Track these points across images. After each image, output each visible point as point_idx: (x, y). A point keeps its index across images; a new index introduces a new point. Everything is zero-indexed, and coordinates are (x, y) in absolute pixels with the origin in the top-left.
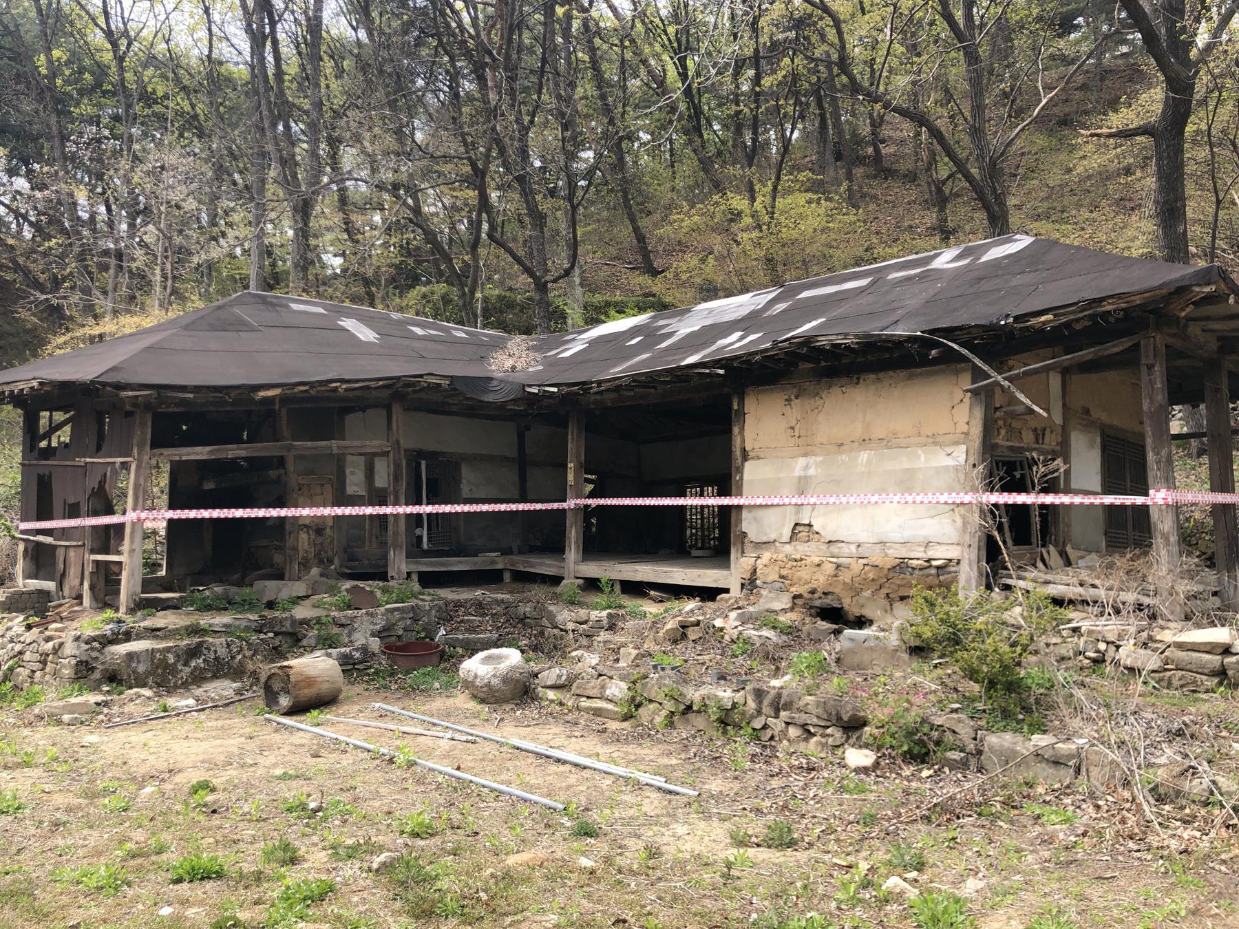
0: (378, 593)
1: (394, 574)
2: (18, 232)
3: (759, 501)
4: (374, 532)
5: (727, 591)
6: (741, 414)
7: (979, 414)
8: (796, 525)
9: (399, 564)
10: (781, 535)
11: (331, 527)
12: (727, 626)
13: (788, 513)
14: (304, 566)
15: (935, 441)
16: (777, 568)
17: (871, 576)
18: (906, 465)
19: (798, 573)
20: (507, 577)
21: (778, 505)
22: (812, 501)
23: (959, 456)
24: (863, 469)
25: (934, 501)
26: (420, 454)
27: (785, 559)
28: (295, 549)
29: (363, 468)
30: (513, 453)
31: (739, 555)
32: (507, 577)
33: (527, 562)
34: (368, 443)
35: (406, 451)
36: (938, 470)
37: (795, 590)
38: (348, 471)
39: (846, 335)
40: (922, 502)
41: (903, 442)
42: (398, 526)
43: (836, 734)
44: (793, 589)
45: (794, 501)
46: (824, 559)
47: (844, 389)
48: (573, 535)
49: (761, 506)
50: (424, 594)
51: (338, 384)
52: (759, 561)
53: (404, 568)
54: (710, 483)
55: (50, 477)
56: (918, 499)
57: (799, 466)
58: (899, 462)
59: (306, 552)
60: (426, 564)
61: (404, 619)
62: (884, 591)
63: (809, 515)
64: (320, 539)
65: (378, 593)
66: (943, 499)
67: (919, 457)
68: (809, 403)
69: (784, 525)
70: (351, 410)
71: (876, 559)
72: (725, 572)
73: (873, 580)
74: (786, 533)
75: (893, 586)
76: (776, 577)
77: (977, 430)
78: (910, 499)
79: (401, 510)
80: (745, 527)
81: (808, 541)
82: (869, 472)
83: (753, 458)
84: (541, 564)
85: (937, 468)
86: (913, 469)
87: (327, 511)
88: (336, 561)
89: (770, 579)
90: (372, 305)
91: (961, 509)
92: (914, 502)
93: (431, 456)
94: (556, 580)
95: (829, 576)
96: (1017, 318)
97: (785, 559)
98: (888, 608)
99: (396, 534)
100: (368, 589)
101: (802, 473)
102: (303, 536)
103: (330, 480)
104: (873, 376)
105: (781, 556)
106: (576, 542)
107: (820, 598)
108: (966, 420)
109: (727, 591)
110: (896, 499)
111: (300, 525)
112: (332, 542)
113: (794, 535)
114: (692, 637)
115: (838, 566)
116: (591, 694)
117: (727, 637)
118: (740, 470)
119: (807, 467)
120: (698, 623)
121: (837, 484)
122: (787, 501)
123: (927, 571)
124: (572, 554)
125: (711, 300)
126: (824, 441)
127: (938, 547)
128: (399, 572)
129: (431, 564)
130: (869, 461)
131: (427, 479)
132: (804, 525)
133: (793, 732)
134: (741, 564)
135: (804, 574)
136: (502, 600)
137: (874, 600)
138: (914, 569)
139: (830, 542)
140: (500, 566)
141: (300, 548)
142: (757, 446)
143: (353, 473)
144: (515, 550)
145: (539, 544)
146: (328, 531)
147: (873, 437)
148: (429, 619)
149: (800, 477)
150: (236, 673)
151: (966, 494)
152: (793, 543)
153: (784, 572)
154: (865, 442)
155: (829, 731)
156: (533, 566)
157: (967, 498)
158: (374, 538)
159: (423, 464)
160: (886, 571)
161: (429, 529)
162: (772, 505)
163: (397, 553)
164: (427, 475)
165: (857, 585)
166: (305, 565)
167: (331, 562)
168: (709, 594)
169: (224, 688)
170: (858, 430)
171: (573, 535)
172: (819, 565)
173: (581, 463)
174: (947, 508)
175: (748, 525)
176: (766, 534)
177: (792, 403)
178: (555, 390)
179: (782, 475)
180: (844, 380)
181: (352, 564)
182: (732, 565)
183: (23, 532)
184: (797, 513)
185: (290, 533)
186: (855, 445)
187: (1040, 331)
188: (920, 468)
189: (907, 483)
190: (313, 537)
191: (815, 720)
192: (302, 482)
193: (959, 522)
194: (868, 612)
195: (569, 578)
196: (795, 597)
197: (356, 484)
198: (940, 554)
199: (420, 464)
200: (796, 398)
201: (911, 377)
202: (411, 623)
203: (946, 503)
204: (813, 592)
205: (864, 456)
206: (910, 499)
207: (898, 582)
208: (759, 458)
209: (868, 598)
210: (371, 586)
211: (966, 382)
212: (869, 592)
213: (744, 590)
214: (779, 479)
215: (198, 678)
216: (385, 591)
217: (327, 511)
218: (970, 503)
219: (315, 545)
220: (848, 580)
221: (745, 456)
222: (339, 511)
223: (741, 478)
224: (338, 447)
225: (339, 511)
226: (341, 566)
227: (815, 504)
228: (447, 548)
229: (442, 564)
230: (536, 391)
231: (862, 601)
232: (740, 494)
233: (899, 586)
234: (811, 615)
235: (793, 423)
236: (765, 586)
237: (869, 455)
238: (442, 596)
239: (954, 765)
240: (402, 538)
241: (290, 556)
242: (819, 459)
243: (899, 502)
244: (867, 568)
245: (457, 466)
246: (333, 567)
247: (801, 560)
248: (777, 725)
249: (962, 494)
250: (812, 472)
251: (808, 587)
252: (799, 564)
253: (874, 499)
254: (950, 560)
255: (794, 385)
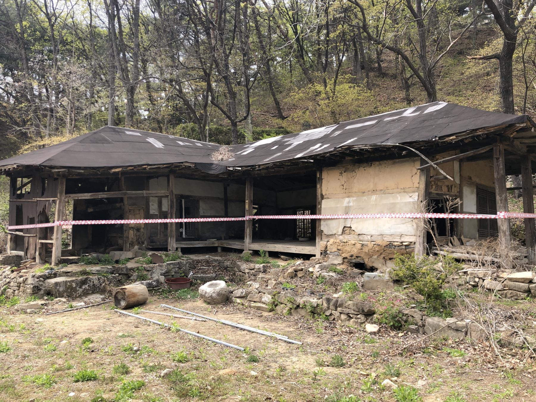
0: (164, 257)
1: (170, 248)
2: (8, 100)
3: (328, 217)
4: (162, 230)
5: (314, 256)
6: (321, 179)
7: (423, 179)
8: (345, 227)
9: (173, 244)
10: (338, 232)
11: (143, 228)
12: (315, 271)
13: (341, 222)
14: (132, 245)
15: (404, 191)
16: (336, 246)
17: (377, 249)
18: (392, 201)
19: (345, 248)
20: (219, 250)
21: (336, 219)
22: (351, 217)
23: (415, 197)
24: (373, 203)
25: (404, 217)
26: (182, 197)
27: (339, 242)
28: (128, 238)
29: (157, 203)
30: (222, 196)
31: (320, 240)
32: (219, 250)
33: (228, 243)
34: (159, 192)
35: (176, 195)
36: (406, 203)
37: (344, 255)
38: (150, 204)
39: (366, 145)
40: (399, 217)
41: (390, 191)
42: (172, 228)
43: (362, 318)
44: (343, 255)
45: (343, 217)
46: (356, 242)
47: (365, 168)
48: (248, 231)
49: (329, 219)
50: (183, 257)
51: (146, 166)
52: (328, 243)
53: (175, 246)
54: (307, 209)
55: (22, 206)
56: (397, 216)
57: (346, 201)
58: (389, 200)
59: (133, 239)
60: (184, 244)
61: (175, 268)
62: (383, 256)
63: (350, 223)
64: (138, 233)
65: (164, 257)
66: (408, 216)
67: (398, 198)
68: (350, 174)
69: (339, 227)
70: (152, 177)
71: (379, 242)
72: (314, 248)
73: (378, 251)
74: (340, 230)
75: (386, 254)
76: (336, 250)
77: (422, 186)
78: (394, 216)
79: (174, 221)
80: (322, 228)
81: (350, 234)
82: (376, 204)
83: (326, 198)
84: (234, 244)
85: (405, 202)
86: (395, 203)
87: (142, 221)
88: (145, 243)
89: (333, 250)
90: (161, 132)
91: (416, 220)
92: (395, 217)
93: (187, 197)
94: (241, 251)
95: (359, 249)
96: (440, 138)
97: (339, 242)
98: (384, 263)
99: (171, 231)
100: (159, 255)
101: (347, 205)
102: (131, 232)
103: (143, 207)
104: (377, 163)
105: (338, 241)
106: (249, 235)
107: (355, 259)
108: (418, 182)
109: (314, 256)
110: (388, 216)
111: (130, 227)
112: (143, 234)
113: (343, 232)
114: (299, 275)
115: (363, 245)
116: (255, 300)
117: (314, 276)
118: (320, 203)
119: (349, 202)
120: (302, 270)
121: (362, 210)
122: (340, 217)
123: (401, 247)
124: (248, 240)
125: (308, 130)
126: (357, 191)
127: (406, 237)
128: (173, 247)
129: (187, 244)
130: (376, 200)
131: (185, 207)
132: (348, 227)
133: (343, 317)
134: (320, 244)
135: (348, 248)
136: (217, 260)
137: (378, 260)
138: (395, 246)
139: (359, 234)
140: (216, 245)
141: (130, 237)
142: (327, 193)
143: (153, 205)
144: (223, 238)
145: (233, 235)
146: (142, 230)
147: (378, 189)
148: (186, 268)
149: (346, 207)
150: (102, 291)
151: (418, 214)
152: (343, 235)
153: (339, 248)
154: (374, 191)
155: (359, 316)
156: (230, 245)
157: (418, 216)
158: (162, 233)
159: (183, 201)
160: (383, 247)
161: (185, 229)
162: (334, 219)
163: (172, 239)
164: (185, 205)
165: (371, 253)
166: (132, 245)
167: (143, 243)
168: (307, 257)
169: (97, 298)
170: (371, 186)
171: (248, 231)
172: (354, 245)
173: (251, 200)
174: (410, 220)
175: (324, 227)
176: (331, 231)
177: (343, 174)
178: (240, 169)
179: (338, 206)
180: (365, 164)
181: (152, 244)
182: (317, 245)
183: (10, 230)
184: (345, 222)
185: (125, 231)
186: (370, 192)
187: (450, 143)
188: (398, 203)
189: (392, 209)
190: (135, 232)
191: (353, 312)
192: (131, 209)
193: (415, 226)
194: (375, 265)
195: (246, 250)
196: (344, 258)
197: (154, 210)
198: (407, 240)
199: (182, 201)
200: (345, 172)
201: (394, 163)
202: (178, 270)
203: (409, 218)
204: (352, 256)
205: (374, 197)
206: (394, 216)
207: (389, 252)
208: (328, 198)
209: (376, 259)
210: (160, 254)
211: (418, 165)
212: (376, 256)
213: (322, 255)
214: (337, 207)
215: (86, 293)
216: (166, 256)
217: (142, 221)
218: (420, 218)
219: (136, 236)
220: (367, 251)
221: (322, 197)
222: (147, 221)
223: (321, 207)
224: (146, 194)
225: (147, 221)
226: (147, 245)
227: (352, 218)
228: (193, 237)
229: (191, 244)
230: (232, 169)
231: (373, 260)
232: (320, 214)
233: (389, 254)
234: (351, 266)
235: (343, 183)
236: (331, 253)
237: (376, 197)
238: (191, 258)
239: (413, 331)
240: (174, 233)
241: (125, 241)
242: (354, 198)
243: (389, 217)
244: (375, 246)
245: (198, 202)
246: (144, 245)
247: (347, 242)
248: (336, 314)
249: (416, 214)
250: (351, 204)
251: (350, 254)
252: (346, 244)
253: (378, 216)
254: (411, 242)
255: (343, 167)
